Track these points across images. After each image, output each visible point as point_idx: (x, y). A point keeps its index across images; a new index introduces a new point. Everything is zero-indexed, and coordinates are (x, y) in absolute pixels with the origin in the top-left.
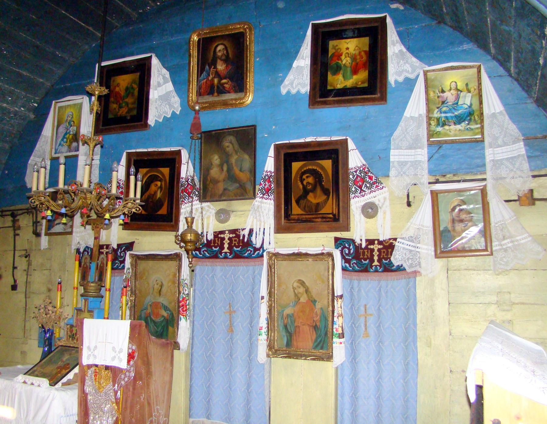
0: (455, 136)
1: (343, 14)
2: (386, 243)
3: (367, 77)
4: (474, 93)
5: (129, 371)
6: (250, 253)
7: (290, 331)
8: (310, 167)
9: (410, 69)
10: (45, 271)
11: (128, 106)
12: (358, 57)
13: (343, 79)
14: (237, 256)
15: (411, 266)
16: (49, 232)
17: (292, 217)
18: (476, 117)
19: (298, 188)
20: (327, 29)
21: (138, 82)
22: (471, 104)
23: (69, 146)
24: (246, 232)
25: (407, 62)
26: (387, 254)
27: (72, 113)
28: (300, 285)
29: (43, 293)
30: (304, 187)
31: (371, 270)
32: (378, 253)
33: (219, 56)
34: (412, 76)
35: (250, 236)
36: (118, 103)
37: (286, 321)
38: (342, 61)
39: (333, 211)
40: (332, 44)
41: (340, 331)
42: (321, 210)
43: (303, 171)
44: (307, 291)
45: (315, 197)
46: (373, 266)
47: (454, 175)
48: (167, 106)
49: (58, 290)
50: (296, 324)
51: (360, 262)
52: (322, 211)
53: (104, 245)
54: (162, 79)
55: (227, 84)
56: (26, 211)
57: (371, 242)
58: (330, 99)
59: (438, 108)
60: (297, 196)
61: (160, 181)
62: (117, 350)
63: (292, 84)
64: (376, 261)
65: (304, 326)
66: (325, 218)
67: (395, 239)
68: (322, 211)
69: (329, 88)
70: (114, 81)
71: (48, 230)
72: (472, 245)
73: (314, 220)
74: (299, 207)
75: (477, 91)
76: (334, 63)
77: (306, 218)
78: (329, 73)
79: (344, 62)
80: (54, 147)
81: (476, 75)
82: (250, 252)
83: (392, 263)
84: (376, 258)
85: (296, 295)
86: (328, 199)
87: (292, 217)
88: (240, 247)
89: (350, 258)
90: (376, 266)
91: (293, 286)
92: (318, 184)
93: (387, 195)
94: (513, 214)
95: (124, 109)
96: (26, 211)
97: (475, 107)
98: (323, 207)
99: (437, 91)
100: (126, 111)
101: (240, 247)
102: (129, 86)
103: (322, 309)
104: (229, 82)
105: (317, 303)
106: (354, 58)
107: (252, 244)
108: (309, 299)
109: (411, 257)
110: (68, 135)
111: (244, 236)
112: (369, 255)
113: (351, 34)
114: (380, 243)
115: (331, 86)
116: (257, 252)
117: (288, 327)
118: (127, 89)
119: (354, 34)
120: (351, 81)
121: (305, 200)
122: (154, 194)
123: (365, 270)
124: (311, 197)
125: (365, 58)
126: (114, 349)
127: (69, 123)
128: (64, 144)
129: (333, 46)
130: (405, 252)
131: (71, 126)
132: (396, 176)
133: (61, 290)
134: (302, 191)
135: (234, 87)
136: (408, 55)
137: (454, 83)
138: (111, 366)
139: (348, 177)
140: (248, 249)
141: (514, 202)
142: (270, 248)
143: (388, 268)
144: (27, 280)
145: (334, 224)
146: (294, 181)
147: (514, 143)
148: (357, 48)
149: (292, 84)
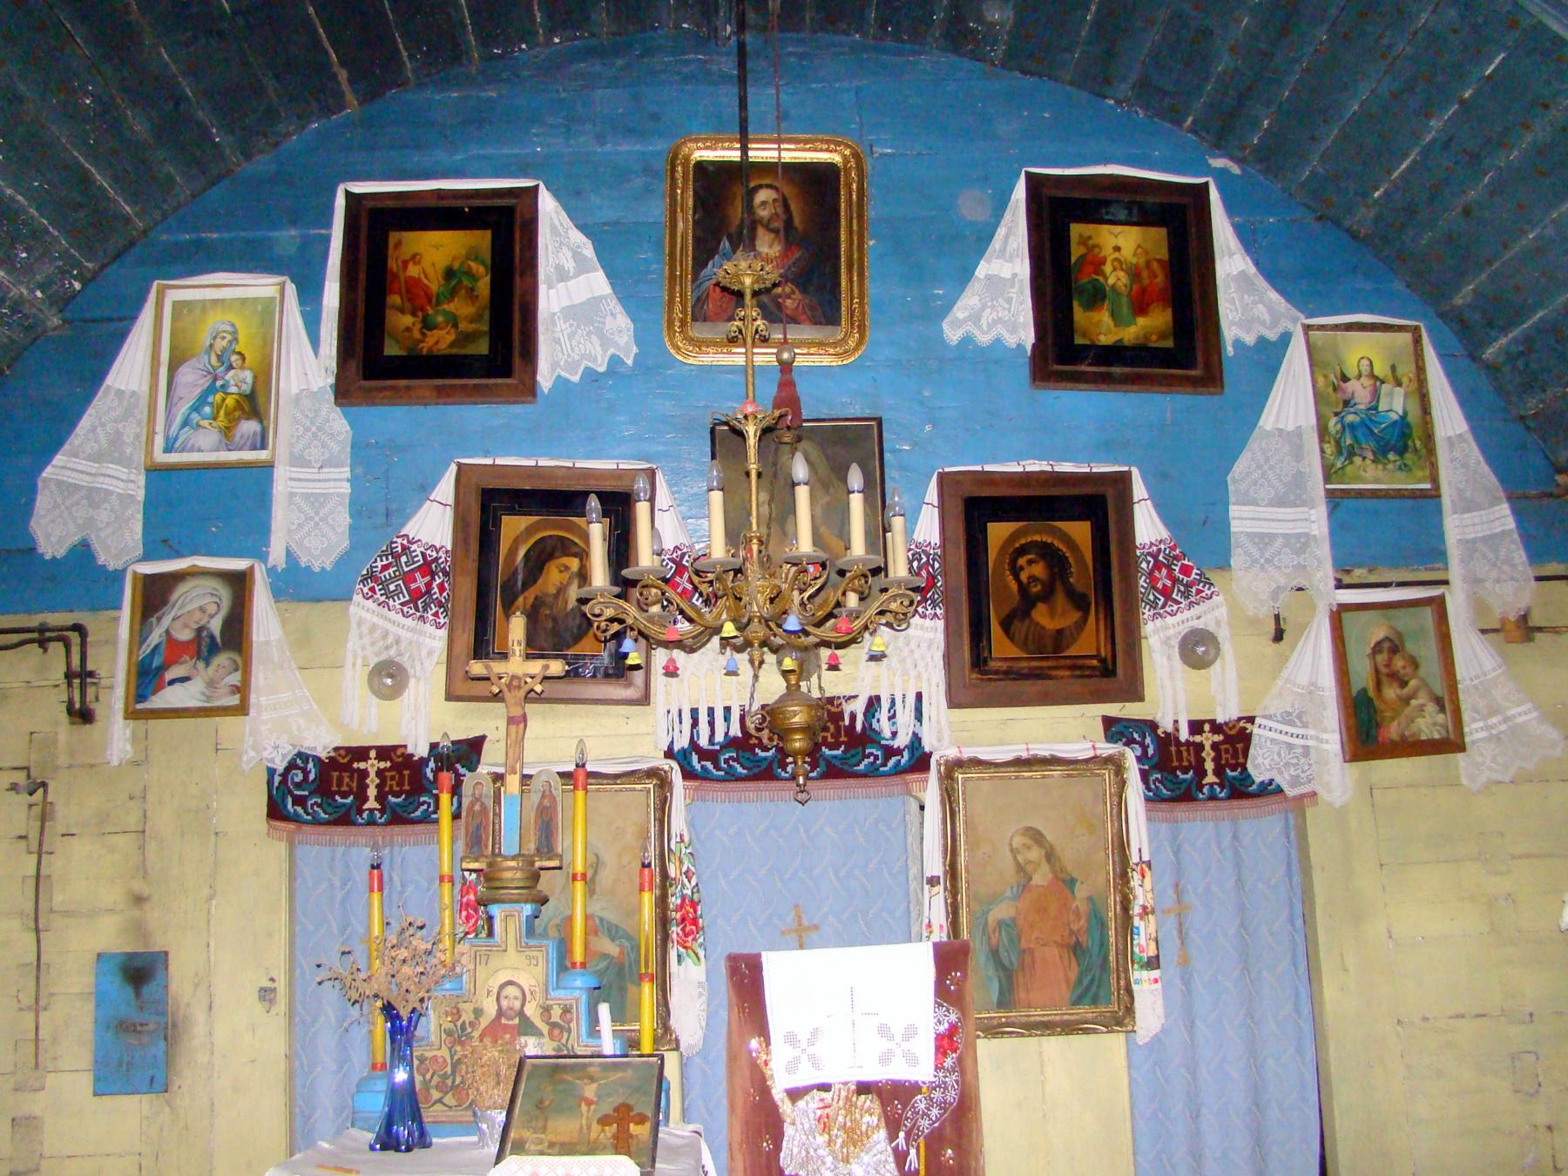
0: (1376, 481)
1: (1106, 162)
2: (1231, 729)
3: (1171, 325)
4: (1410, 389)
5: (943, 1086)
6: (872, 764)
7: (1006, 962)
8: (1037, 538)
9: (1267, 317)
10: (115, 838)
11: (456, 325)
12: (1145, 274)
13: (1111, 323)
14: (834, 772)
15: (1295, 782)
16: (140, 706)
17: (993, 665)
18: (1418, 443)
19: (1004, 588)
20: (1060, 194)
21: (488, 261)
22: (1405, 413)
23: (227, 432)
24: (859, 707)
25: (1261, 301)
26: (1235, 755)
27: (233, 325)
28: (1030, 842)
29: (111, 911)
30: (1023, 589)
31: (1201, 796)
32: (377, 781)
33: (762, 218)
34: (1272, 335)
35: (870, 716)
36: (420, 314)
37: (994, 941)
38: (1106, 278)
39: (1098, 650)
40: (1077, 230)
41: (1152, 951)
42: (1068, 648)
43: (1017, 545)
44: (1050, 856)
45: (1052, 614)
46: (1203, 786)
47: (1370, 571)
48: (594, 339)
49: (372, 890)
50: (1023, 945)
51: (1170, 777)
52: (1072, 652)
53: (370, 748)
54: (571, 260)
55: (788, 297)
56: (35, 635)
57: (1196, 727)
58: (1083, 368)
59: (1336, 414)
60: (1006, 611)
61: (575, 555)
62: (898, 1030)
63: (975, 318)
64: (1210, 772)
65: (1046, 949)
66: (1081, 668)
67: (1251, 720)
68: (1072, 652)
69: (1079, 340)
70: (398, 244)
71: (138, 702)
72: (1421, 731)
73: (1054, 673)
74: (1012, 639)
75: (1414, 385)
76: (1085, 280)
77: (1030, 668)
78: (1075, 304)
79: (1111, 281)
80: (160, 428)
81: (1411, 348)
82: (872, 759)
83: (1249, 776)
84: (1209, 766)
85: (1020, 868)
86: (1085, 619)
87: (993, 665)
88: (843, 748)
89: (306, 793)
90: (1211, 785)
91: (1011, 845)
92: (1058, 583)
93: (1223, 611)
94: (1499, 660)
95: (442, 333)
96: (35, 635)
97: (1414, 417)
98: (1074, 640)
99: (1332, 377)
100: (451, 338)
101: (843, 748)
102: (456, 266)
103: (1090, 899)
104: (793, 293)
105: (1078, 884)
106: (1135, 273)
107: (877, 739)
108: (1056, 877)
109: (1295, 761)
110: (219, 397)
111: (853, 717)
112: (1192, 759)
113: (1122, 215)
114: (1216, 728)
115: (1084, 335)
116: (893, 760)
117: (1003, 954)
118: (449, 273)
119: (1130, 214)
120: (1133, 331)
121: (1027, 622)
122: (559, 592)
123: (344, 819)
124: (1040, 614)
125: (1160, 279)
126: (884, 1031)
127: (219, 357)
128: (205, 423)
129: (1081, 236)
130: (1276, 748)
131: (231, 367)
132: (1246, 569)
133: (381, 889)
134: (1018, 598)
135: (812, 308)
136: (1261, 282)
137: (1365, 362)
138: (877, 1083)
139: (1137, 565)
140: (867, 751)
141: (1494, 634)
142: (941, 748)
143: (1240, 790)
144: (38, 869)
145: (1104, 683)
146: (994, 569)
147: (1492, 505)
148: (1139, 250)
149: (975, 318)
